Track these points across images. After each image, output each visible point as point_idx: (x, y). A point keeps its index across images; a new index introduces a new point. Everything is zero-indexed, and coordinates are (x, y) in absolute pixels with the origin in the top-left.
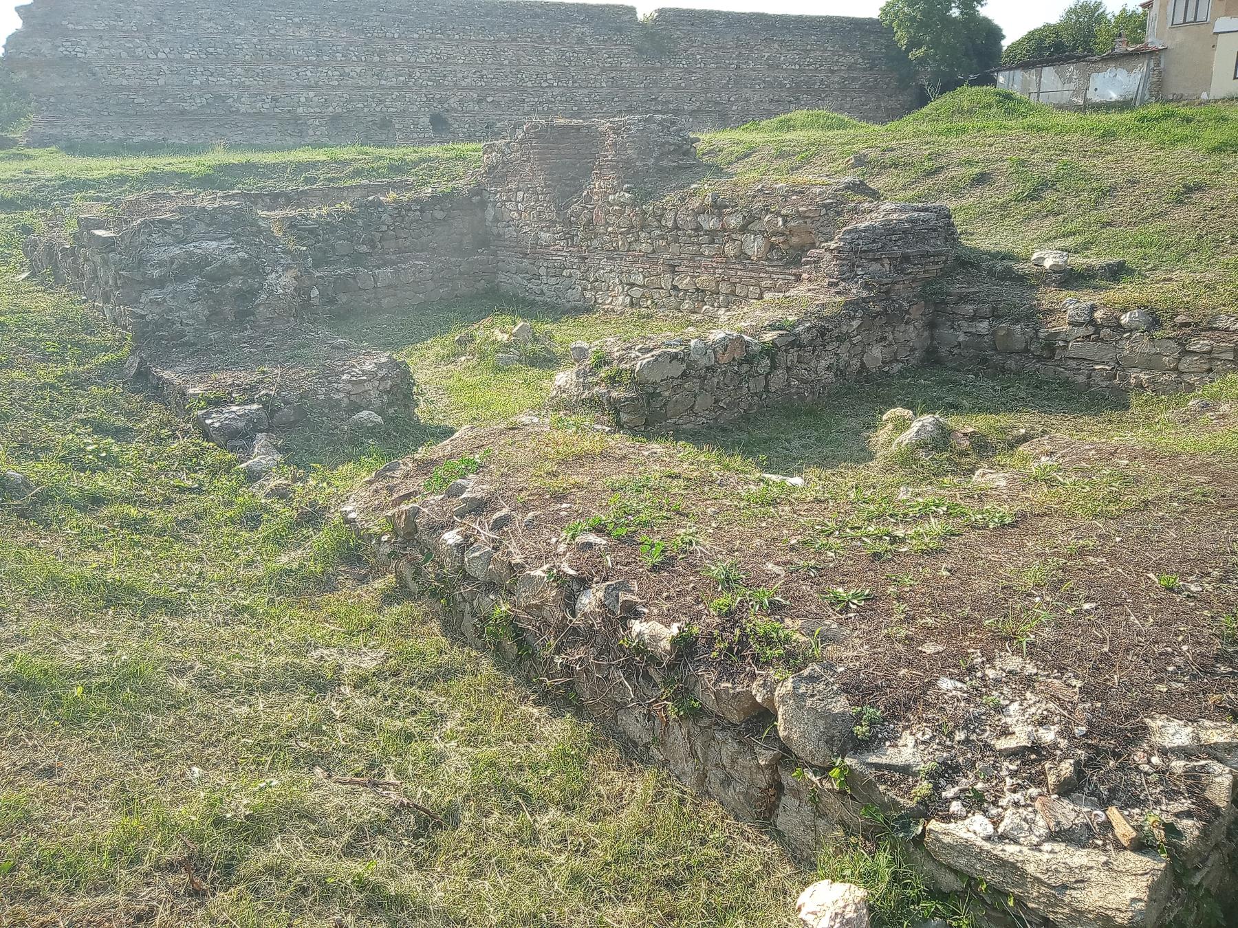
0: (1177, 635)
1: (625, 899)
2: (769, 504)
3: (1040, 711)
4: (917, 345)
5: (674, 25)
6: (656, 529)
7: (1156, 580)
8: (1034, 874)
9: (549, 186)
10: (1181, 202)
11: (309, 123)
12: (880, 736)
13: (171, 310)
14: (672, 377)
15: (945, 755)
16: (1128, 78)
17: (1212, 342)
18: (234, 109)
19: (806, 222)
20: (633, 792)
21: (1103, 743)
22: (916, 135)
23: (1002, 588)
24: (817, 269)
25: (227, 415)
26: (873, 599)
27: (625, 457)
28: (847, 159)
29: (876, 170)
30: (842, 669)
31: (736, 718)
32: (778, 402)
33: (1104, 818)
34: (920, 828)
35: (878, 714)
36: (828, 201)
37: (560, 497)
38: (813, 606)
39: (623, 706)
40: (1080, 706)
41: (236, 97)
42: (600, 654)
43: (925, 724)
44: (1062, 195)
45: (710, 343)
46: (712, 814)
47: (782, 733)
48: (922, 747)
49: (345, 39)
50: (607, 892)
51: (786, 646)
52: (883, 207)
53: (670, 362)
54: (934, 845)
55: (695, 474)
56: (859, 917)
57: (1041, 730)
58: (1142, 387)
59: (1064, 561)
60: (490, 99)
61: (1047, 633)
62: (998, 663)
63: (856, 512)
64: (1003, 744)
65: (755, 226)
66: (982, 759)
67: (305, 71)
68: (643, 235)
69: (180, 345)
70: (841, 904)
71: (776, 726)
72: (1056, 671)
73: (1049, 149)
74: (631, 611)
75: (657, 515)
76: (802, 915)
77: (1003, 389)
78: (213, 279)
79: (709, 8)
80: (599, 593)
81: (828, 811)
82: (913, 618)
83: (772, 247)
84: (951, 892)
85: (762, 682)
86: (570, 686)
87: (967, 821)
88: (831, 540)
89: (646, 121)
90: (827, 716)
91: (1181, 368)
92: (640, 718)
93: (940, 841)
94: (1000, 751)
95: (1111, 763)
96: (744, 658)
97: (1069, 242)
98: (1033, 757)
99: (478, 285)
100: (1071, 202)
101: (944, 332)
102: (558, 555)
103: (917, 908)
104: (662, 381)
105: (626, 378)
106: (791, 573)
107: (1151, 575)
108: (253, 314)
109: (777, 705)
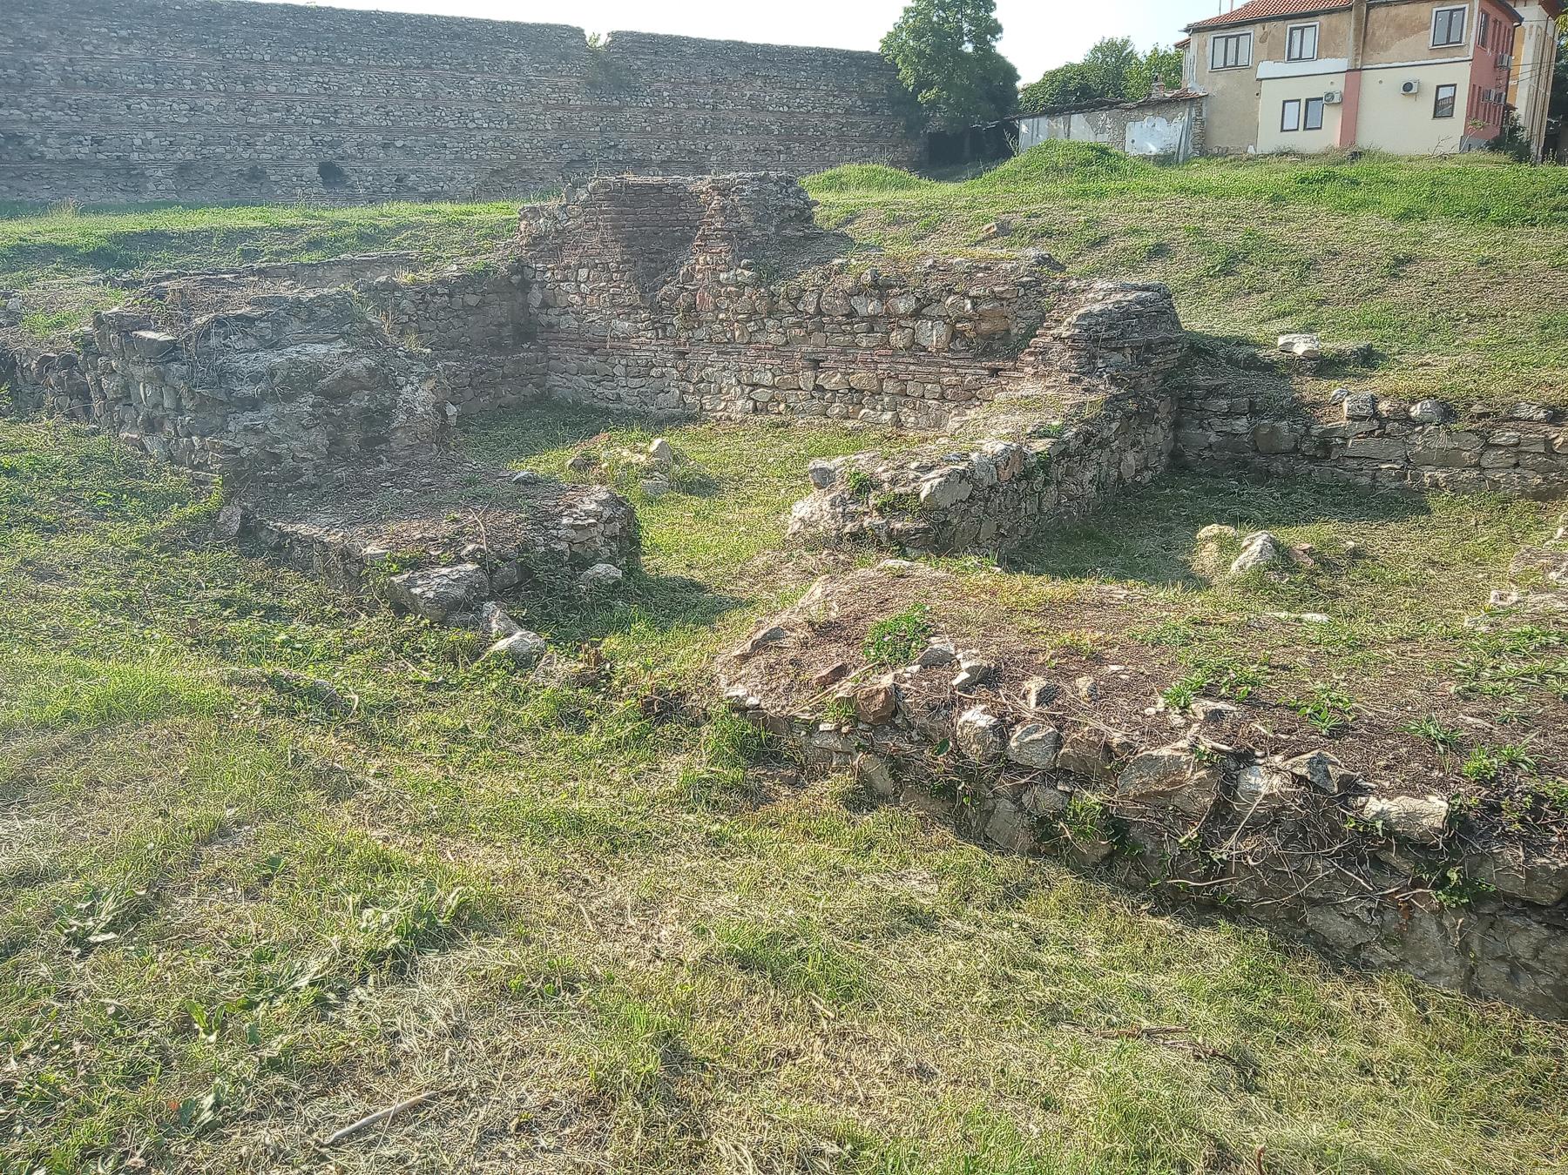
5: (632, 53)
9: (627, 261)
10: (1395, 275)
11: (147, 173)
13: (277, 441)
16: (1167, 129)
17: (1519, 434)
18: (37, 154)
24: (1047, 363)
25: (438, 581)
29: (1026, 239)
36: (1025, 279)
41: (38, 137)
49: (195, 61)
58: (1437, 486)
60: (399, 143)
65: (934, 310)
67: (139, 104)
69: (297, 488)
73: (1219, 215)
78: (331, 395)
79: (675, 32)
83: (955, 335)
89: (761, 179)
91: (1484, 464)
99: (526, 391)
101: (1193, 432)
104: (952, 505)
108: (387, 441)
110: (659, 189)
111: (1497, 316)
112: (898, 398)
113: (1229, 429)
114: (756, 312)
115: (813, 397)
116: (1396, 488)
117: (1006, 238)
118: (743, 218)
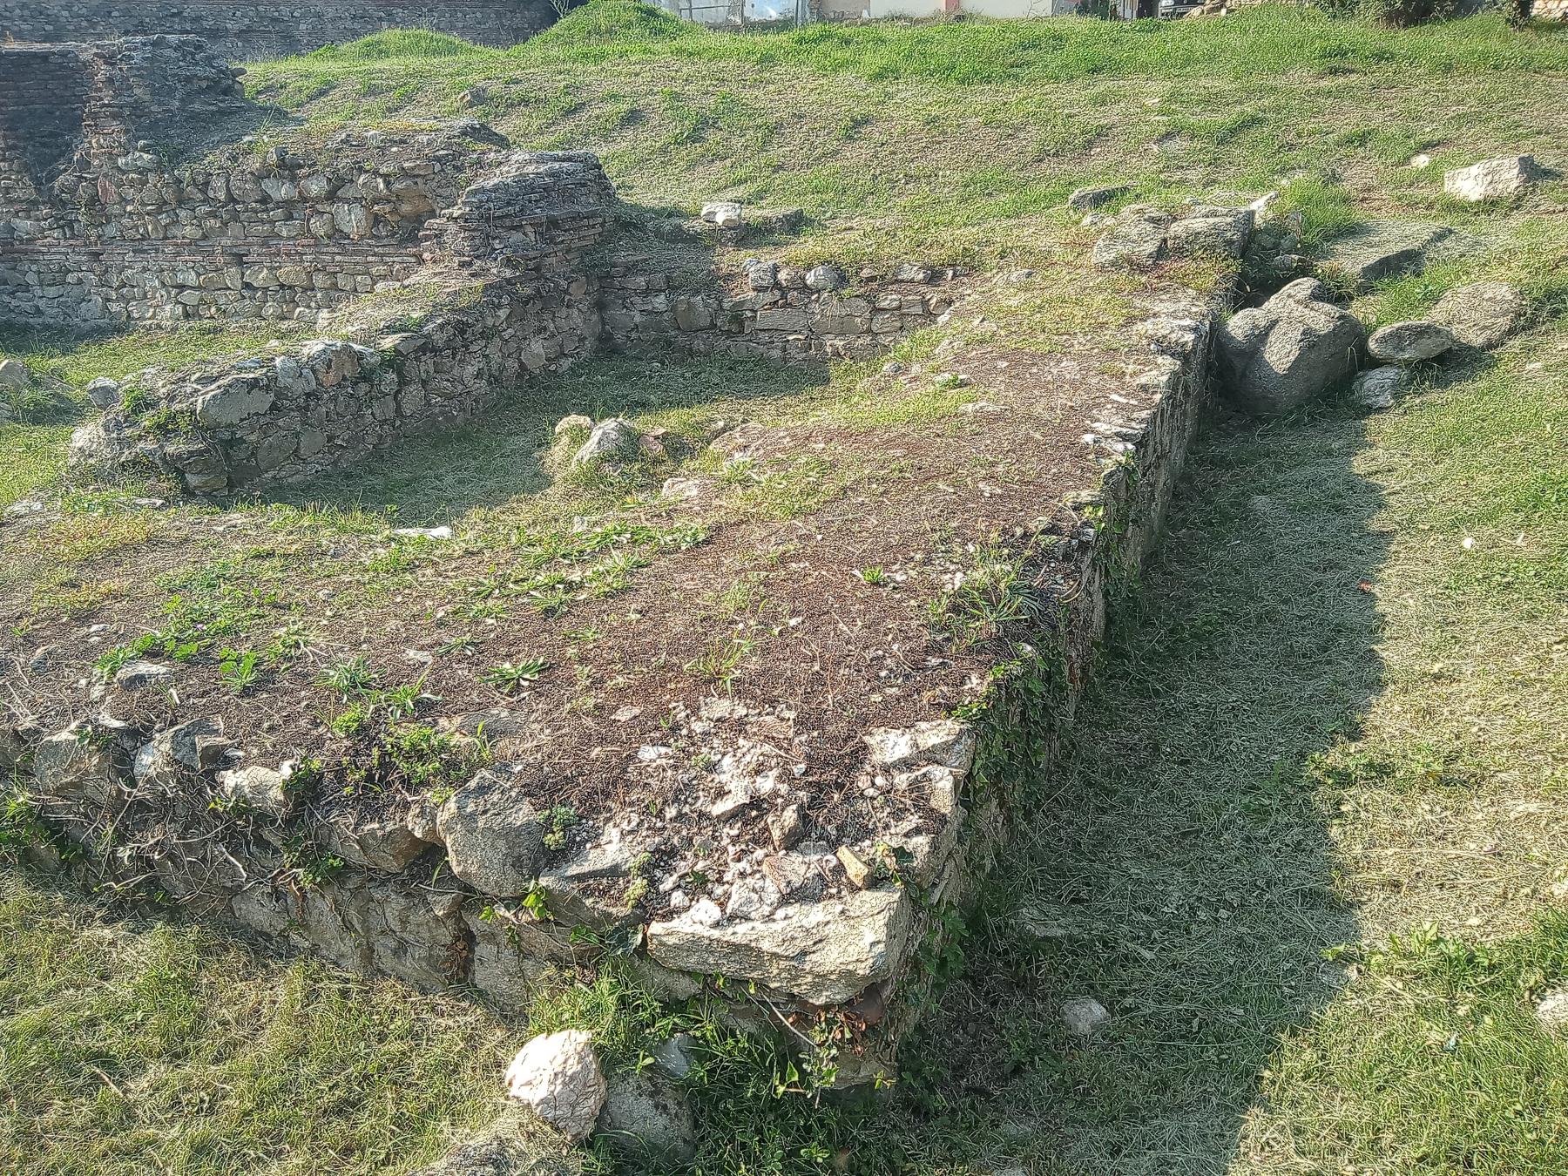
0: (886, 635)
1: (281, 1152)
2: (404, 570)
3: (755, 758)
4: (587, 333)
6: (243, 635)
7: (861, 576)
8: (770, 951)
10: (850, 137)
12: (578, 839)
14: (257, 414)
15: (657, 840)
19: (416, 183)
20: (274, 1002)
21: (824, 777)
22: (546, 61)
23: (701, 621)
26: (550, 668)
27: (186, 540)
28: (462, 94)
30: (520, 768)
31: (394, 867)
32: (417, 428)
33: (834, 862)
34: (640, 936)
35: (572, 813)
36: (442, 152)
37: (85, 617)
38: (474, 695)
39: (236, 891)
40: (797, 741)
42: (186, 829)
43: (629, 809)
44: (726, 135)
45: (305, 359)
46: (389, 997)
47: (456, 870)
48: (629, 838)
50: (251, 1152)
51: (442, 756)
52: (514, 158)
53: (249, 393)
54: (659, 951)
55: (294, 547)
56: (586, 1068)
57: (759, 779)
59: (765, 573)
61: (754, 664)
62: (704, 713)
63: (519, 560)
64: (719, 808)
65: (347, 192)
66: (699, 833)
68: (183, 214)
70: (562, 1058)
71: (447, 862)
72: (767, 706)
74: (219, 760)
75: (243, 615)
76: (513, 1091)
77: (695, 375)
80: (163, 745)
81: (533, 949)
82: (602, 681)
83: (377, 220)
84: (689, 998)
85: (418, 810)
86: (153, 884)
87: (692, 911)
88: (490, 602)
89: (154, 44)
90: (511, 834)
91: (874, 329)
92: (265, 901)
93: (664, 945)
94: (718, 817)
95: (836, 796)
96: (389, 784)
97: (741, 192)
98: (754, 813)
100: (737, 143)
101: (617, 313)
102: (93, 704)
103: (653, 1031)
104: (242, 420)
105: (183, 423)
106: (441, 657)
107: (856, 572)
109: (442, 835)
110: (44, 57)
111: (930, 176)
112: (332, 293)
113: (650, 308)
114: (165, 203)
115: (244, 297)
116: (804, 360)
117: (480, 107)
118: (137, 91)
